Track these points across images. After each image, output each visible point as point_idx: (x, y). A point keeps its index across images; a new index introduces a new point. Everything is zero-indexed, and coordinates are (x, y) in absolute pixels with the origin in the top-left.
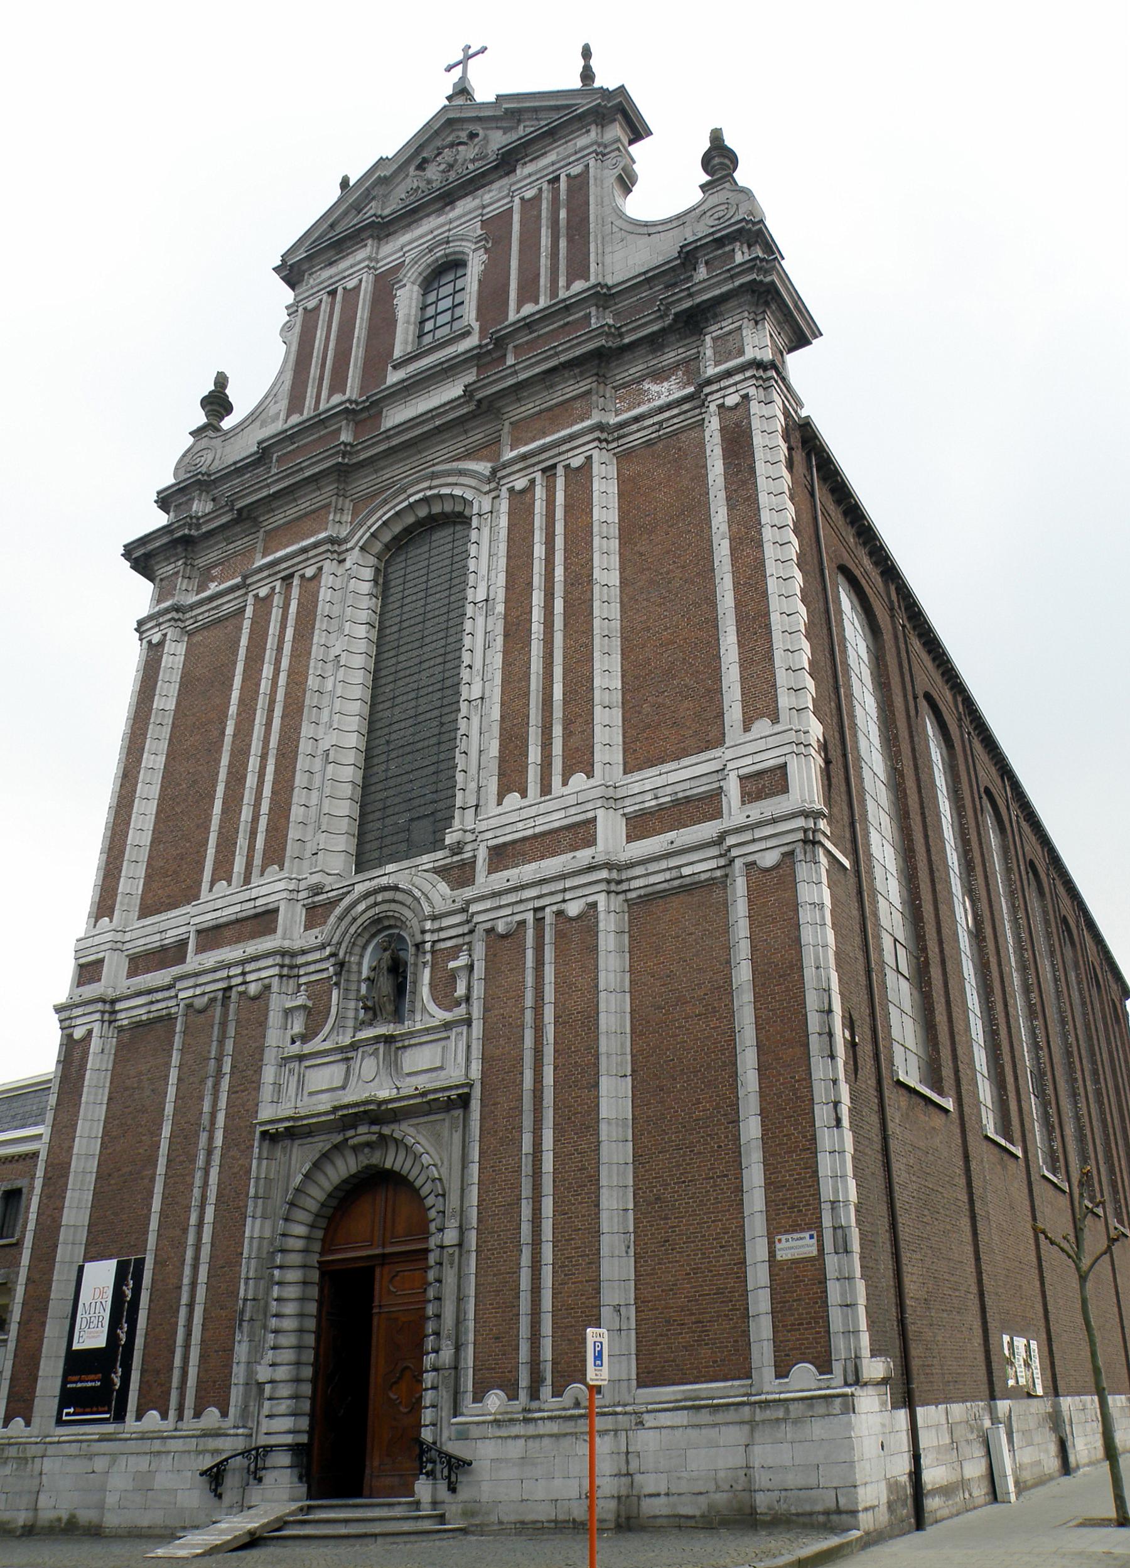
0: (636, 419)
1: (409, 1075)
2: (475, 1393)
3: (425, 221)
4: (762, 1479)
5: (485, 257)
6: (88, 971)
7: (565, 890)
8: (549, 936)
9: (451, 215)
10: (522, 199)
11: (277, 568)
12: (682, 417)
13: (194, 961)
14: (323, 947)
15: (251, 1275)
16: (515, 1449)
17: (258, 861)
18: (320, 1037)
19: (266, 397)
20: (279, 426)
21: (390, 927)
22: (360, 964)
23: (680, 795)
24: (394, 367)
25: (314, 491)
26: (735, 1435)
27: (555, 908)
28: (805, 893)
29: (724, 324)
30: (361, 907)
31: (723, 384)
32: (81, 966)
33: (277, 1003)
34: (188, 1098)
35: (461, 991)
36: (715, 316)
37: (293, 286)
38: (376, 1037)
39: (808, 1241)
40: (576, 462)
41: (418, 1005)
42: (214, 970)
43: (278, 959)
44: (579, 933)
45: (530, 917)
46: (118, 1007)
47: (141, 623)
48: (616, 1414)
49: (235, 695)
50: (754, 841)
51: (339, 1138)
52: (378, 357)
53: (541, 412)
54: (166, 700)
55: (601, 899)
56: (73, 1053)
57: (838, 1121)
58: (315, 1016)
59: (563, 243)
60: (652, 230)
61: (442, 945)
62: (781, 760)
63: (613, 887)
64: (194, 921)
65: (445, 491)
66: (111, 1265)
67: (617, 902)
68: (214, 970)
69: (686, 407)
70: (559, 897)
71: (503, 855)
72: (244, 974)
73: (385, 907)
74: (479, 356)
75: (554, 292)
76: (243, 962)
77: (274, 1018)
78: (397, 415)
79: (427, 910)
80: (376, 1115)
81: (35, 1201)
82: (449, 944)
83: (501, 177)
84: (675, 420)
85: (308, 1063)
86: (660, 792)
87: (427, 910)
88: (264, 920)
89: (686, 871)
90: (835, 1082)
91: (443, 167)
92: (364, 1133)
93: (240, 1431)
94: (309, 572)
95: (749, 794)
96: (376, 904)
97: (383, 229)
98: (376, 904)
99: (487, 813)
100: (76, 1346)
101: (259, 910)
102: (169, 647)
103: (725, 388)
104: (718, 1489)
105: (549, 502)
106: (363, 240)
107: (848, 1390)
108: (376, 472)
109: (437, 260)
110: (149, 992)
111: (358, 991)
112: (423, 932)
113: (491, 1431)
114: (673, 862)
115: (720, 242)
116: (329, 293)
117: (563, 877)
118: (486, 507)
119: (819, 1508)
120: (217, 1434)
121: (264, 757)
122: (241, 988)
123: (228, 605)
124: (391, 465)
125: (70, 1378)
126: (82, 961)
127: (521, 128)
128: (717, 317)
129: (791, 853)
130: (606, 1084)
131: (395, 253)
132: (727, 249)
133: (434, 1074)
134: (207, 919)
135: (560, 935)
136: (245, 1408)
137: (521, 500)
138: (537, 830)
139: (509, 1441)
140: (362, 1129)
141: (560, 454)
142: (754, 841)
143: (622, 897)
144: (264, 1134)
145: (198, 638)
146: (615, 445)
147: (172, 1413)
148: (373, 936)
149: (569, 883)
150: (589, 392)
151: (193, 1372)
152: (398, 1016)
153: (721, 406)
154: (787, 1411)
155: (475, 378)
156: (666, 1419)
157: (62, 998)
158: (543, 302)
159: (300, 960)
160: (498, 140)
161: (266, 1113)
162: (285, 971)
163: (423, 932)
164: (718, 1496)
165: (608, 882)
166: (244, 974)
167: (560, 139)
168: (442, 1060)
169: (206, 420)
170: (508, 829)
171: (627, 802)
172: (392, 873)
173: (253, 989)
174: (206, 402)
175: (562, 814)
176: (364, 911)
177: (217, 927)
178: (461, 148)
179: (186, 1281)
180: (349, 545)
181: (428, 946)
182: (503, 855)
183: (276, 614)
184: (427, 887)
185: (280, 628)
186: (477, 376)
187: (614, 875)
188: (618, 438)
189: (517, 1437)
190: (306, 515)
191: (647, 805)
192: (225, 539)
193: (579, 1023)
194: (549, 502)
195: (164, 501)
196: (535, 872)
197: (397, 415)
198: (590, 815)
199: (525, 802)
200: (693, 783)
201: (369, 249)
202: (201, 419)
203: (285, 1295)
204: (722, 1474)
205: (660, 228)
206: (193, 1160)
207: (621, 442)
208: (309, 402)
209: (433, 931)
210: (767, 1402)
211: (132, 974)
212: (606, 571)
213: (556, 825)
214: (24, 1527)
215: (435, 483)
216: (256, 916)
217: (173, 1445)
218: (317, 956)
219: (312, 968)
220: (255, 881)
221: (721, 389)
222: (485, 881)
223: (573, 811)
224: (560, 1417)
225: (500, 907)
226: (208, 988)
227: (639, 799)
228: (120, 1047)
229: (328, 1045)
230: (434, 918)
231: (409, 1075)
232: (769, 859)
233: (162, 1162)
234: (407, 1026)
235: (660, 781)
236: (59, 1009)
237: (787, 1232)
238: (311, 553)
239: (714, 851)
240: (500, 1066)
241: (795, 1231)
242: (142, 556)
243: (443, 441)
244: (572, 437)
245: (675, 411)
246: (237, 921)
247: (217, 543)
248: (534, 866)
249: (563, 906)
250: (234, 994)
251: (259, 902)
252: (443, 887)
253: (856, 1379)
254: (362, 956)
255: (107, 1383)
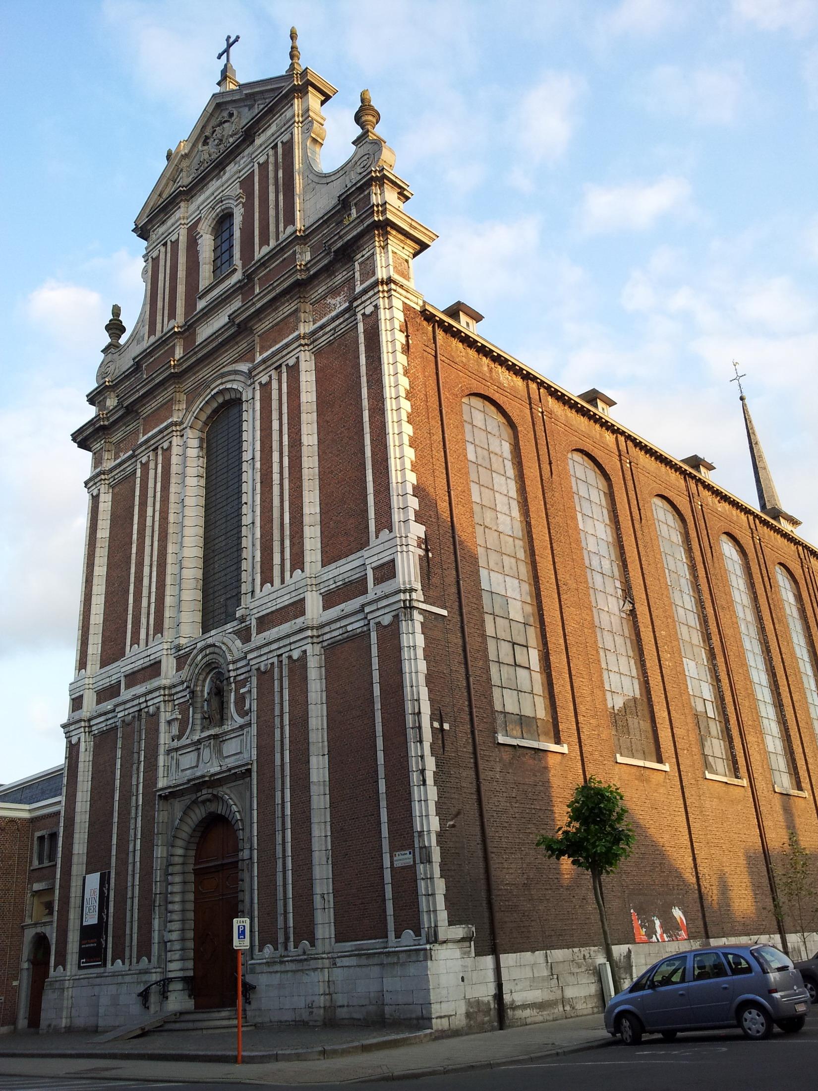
0: (322, 328)
1: (227, 757)
2: (259, 946)
3: (210, 184)
4: (387, 998)
5: (243, 210)
6: (77, 703)
7: (290, 644)
8: (285, 672)
9: (225, 178)
10: (258, 163)
11: (149, 444)
12: (345, 323)
13: (126, 694)
14: (182, 683)
15: (158, 879)
16: (276, 979)
17: (151, 632)
18: (185, 737)
19: (138, 323)
20: (145, 344)
21: (215, 668)
22: (202, 691)
23: (347, 580)
24: (200, 298)
25: (163, 391)
26: (375, 971)
27: (287, 654)
28: (405, 640)
29: (364, 252)
30: (199, 657)
31: (364, 298)
32: (73, 700)
33: (164, 717)
34: (126, 776)
35: (247, 707)
36: (358, 248)
37: (146, 240)
38: (208, 736)
39: (408, 856)
40: (291, 362)
41: (229, 715)
42: (132, 700)
43: (162, 692)
44: (299, 667)
45: (275, 660)
46: (92, 723)
47: (86, 483)
48: (323, 958)
49: (135, 527)
50: (378, 609)
51: (194, 797)
52: (193, 293)
53: (273, 326)
54: (103, 533)
55: (309, 648)
56: (72, 751)
57: (424, 781)
58: (184, 725)
59: (281, 197)
60: (329, 180)
61: (239, 678)
62: (391, 557)
63: (315, 640)
64: (123, 670)
65: (229, 386)
66: (97, 875)
67: (317, 648)
68: (132, 700)
69: (347, 316)
70: (288, 648)
71: (265, 622)
72: (146, 701)
73: (211, 656)
74: (240, 288)
75: (277, 239)
76: (145, 695)
77: (163, 727)
78: (204, 332)
79: (230, 658)
80: (213, 782)
81: (61, 839)
82: (242, 677)
83: (248, 146)
84: (342, 326)
85: (180, 753)
86: (337, 579)
87: (230, 658)
88: (154, 668)
89: (349, 628)
90: (422, 757)
91: (217, 141)
92: (205, 793)
93: (158, 970)
94: (165, 445)
95: (377, 579)
96: (206, 655)
97: (188, 193)
98: (206, 655)
99: (259, 599)
100: (84, 924)
101: (152, 662)
102: (102, 498)
103: (365, 301)
104: (371, 1004)
105: (279, 389)
106: (178, 204)
107: (428, 947)
108: (194, 374)
109: (218, 215)
110: (105, 714)
111: (202, 707)
112: (229, 671)
113: (265, 969)
114: (343, 623)
115: (361, 189)
116: (163, 245)
117: (288, 636)
118: (250, 396)
119: (414, 1016)
120: (146, 972)
121: (151, 566)
122: (146, 710)
123: (128, 467)
124: (201, 369)
125: (84, 942)
126: (73, 697)
127: (256, 106)
128: (360, 249)
129: (397, 615)
130: (313, 760)
131: (194, 212)
132: (366, 193)
133: (238, 756)
134: (128, 669)
135: (291, 670)
136: (159, 956)
137: (266, 388)
138: (278, 607)
139: (273, 975)
140: (204, 792)
141: (283, 357)
142: (378, 609)
143: (320, 645)
144: (160, 796)
145: (117, 490)
146: (311, 347)
147: (127, 961)
148: (208, 674)
149: (292, 639)
150: (296, 311)
151: (135, 936)
152: (222, 721)
153: (364, 315)
154: (398, 958)
155: (240, 304)
156: (346, 962)
157: (65, 720)
158: (272, 243)
159: (173, 691)
160: (245, 116)
161: (161, 783)
162: (166, 698)
163: (229, 671)
164: (371, 1007)
165: (312, 637)
166: (146, 701)
167: (277, 113)
168: (240, 750)
169: (110, 340)
170: (264, 607)
171: (322, 586)
172: (215, 636)
173: (152, 710)
174: (108, 328)
175: (288, 597)
176: (202, 660)
177: (134, 673)
178: (226, 125)
179: (129, 884)
180: (185, 426)
181: (232, 679)
182: (265, 622)
183: (152, 473)
184: (230, 644)
185: (154, 485)
186: (243, 301)
187: (315, 633)
188: (313, 342)
189: (277, 972)
190: (162, 406)
191: (331, 587)
192: (124, 424)
193: (300, 723)
194: (279, 389)
195: (92, 399)
196: (277, 633)
197: (204, 332)
198: (302, 596)
199: (274, 589)
200: (353, 572)
201: (182, 210)
202: (106, 340)
203: (175, 890)
204: (372, 995)
205: (333, 178)
206: (129, 813)
207: (315, 344)
208: (159, 326)
209: (234, 670)
210: (389, 952)
211: (99, 702)
212: (310, 437)
213: (286, 603)
214: (65, 1027)
215: (224, 380)
216: (151, 665)
217: (128, 979)
218: (180, 688)
219: (180, 695)
220: (151, 644)
221: (362, 303)
222: (257, 639)
223: (293, 594)
224: (296, 960)
225: (261, 655)
226: (131, 710)
227: (327, 584)
228: (96, 747)
229: (189, 741)
230: (234, 662)
231: (227, 757)
232: (387, 620)
233: (116, 814)
234: (226, 728)
235: (336, 572)
236: (64, 726)
237: (399, 850)
238: (165, 433)
239: (361, 616)
240: (265, 750)
241: (402, 850)
242: (84, 438)
243: (226, 351)
244: (287, 345)
245: (341, 320)
246: (143, 669)
247: (121, 427)
248: (276, 629)
249: (291, 653)
250: (144, 715)
251: (152, 657)
252: (238, 643)
253: (434, 939)
254: (203, 686)
255: (100, 943)
